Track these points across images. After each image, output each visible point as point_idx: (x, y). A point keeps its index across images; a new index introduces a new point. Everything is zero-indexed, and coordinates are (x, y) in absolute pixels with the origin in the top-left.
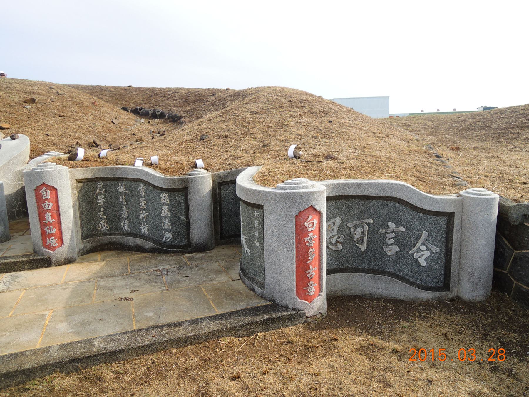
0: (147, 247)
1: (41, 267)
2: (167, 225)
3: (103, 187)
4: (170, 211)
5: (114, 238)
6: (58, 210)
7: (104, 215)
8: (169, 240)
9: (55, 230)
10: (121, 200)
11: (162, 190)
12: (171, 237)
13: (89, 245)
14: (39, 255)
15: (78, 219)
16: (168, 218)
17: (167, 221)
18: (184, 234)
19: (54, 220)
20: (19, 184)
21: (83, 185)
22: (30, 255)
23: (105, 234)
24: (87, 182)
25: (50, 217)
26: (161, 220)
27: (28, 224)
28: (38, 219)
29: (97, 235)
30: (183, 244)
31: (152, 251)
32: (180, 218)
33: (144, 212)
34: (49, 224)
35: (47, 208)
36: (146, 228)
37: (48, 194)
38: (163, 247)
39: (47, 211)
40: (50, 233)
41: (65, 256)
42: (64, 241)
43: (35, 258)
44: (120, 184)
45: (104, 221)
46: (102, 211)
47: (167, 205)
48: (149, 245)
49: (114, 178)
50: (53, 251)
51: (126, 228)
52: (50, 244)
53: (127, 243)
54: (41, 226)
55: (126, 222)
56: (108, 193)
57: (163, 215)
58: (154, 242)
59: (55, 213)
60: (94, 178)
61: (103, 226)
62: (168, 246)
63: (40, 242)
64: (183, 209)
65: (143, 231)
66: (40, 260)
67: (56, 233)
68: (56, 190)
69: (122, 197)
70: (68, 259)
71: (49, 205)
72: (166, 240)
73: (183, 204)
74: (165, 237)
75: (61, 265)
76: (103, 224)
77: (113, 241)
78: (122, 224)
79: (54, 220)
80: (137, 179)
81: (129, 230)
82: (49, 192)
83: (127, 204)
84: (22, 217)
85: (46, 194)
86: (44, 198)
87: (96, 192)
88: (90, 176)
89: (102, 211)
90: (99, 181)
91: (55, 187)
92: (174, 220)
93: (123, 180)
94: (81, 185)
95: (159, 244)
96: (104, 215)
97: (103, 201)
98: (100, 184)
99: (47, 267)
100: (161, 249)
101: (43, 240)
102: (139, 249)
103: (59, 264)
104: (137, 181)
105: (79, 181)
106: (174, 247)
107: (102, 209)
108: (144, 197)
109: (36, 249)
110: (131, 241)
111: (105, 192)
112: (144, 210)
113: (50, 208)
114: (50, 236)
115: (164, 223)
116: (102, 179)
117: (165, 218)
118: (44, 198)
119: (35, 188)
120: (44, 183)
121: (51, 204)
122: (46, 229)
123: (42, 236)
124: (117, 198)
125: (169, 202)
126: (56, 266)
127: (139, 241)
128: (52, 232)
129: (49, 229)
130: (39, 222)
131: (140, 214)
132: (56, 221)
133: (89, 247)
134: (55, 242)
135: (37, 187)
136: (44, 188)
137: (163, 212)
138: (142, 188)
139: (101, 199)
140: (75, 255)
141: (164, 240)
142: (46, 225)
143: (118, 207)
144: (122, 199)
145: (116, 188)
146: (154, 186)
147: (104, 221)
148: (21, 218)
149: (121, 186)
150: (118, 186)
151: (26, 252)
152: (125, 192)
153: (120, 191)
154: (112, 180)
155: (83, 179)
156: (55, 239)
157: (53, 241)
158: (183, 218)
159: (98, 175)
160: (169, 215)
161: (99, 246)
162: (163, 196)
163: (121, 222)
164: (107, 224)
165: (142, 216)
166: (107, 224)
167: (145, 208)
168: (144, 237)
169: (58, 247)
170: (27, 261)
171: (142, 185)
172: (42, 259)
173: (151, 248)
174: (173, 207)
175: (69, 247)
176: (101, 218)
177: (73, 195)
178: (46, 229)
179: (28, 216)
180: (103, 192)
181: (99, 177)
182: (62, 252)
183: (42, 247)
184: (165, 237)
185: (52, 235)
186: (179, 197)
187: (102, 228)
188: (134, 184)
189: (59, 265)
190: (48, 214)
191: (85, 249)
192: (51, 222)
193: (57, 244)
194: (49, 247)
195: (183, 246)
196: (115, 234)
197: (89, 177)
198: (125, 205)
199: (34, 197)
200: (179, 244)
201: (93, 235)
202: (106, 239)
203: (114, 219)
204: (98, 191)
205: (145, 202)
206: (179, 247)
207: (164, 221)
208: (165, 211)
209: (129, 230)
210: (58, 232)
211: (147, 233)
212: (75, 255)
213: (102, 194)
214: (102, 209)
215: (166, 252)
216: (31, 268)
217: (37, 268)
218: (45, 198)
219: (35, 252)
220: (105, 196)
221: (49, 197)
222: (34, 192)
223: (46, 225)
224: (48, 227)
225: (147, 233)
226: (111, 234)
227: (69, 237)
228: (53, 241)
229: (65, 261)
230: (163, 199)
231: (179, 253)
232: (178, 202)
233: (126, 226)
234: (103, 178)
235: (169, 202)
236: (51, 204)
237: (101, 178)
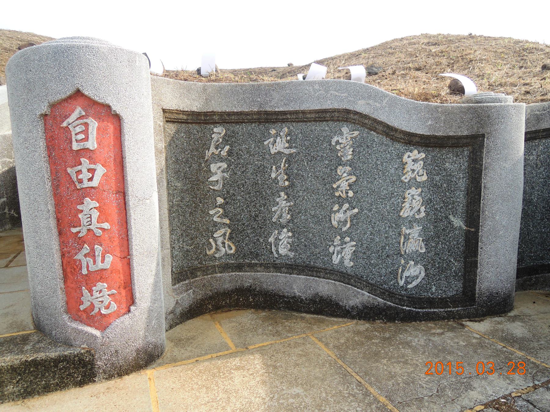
0: (352, 303)
1: (61, 386)
2: (414, 242)
3: (226, 140)
4: (427, 202)
5: (247, 278)
6: (122, 193)
7: (225, 215)
8: (414, 283)
9: (109, 258)
10: (273, 175)
11: (412, 140)
12: (423, 274)
13: (187, 298)
14: (55, 342)
15: (166, 224)
16: (418, 221)
17: (415, 232)
18: (457, 265)
19: (106, 226)
20: (4, 163)
21: (177, 132)
22: (25, 339)
23: (225, 268)
24: (186, 122)
25: (95, 214)
26: (398, 226)
27: (21, 241)
28: (52, 223)
29: (205, 270)
30: (450, 294)
31: (366, 313)
32: (450, 222)
33: (346, 206)
34: (93, 239)
35: (86, 184)
36: (349, 249)
37: (90, 135)
38: (401, 301)
39: (88, 192)
40: (92, 268)
41: (139, 343)
42: (137, 295)
43: (41, 356)
44: (273, 132)
45: (222, 231)
46: (220, 206)
47: (418, 185)
48: (359, 297)
49: (259, 113)
50: (103, 328)
51: (283, 251)
52: (92, 306)
53: (287, 291)
54: (63, 244)
55: (285, 235)
56: (239, 157)
57: (404, 214)
58: (373, 288)
59: (112, 199)
60: (206, 114)
61: (221, 245)
62: (415, 300)
63: (59, 300)
64: (461, 197)
65: (336, 260)
66: (57, 361)
67: (113, 270)
68: (117, 118)
69: (278, 168)
70: (146, 352)
71: (92, 171)
72: (407, 283)
73: (462, 184)
74: (406, 274)
75: (127, 372)
76: (220, 240)
77: (247, 285)
78: (271, 240)
79: (106, 226)
80: (334, 111)
81: (292, 254)
82: (94, 125)
83: (292, 186)
84: (8, 226)
85: (86, 132)
86: (75, 146)
87: (208, 154)
88: (196, 106)
89: (220, 206)
90: (215, 123)
91: (117, 108)
92: (435, 228)
93: (283, 121)
94: (172, 128)
95: (389, 294)
96: (225, 215)
97: (224, 179)
98: (219, 132)
99: (81, 384)
100: (395, 310)
101: (67, 293)
102: (325, 308)
103: (121, 371)
104: (324, 120)
105: (171, 117)
106: (431, 302)
107: (220, 200)
108: (351, 163)
109: (46, 321)
110: (299, 285)
111: (230, 153)
112: (347, 200)
113: (95, 183)
114: (91, 279)
115: (407, 237)
116: (225, 119)
117: (411, 222)
118: (75, 146)
119: (44, 108)
120: (78, 93)
121: (100, 171)
122: (80, 256)
123: (65, 278)
124: (262, 170)
125: (425, 178)
126: (110, 377)
127: (325, 287)
128: (100, 265)
129: (92, 254)
130: (55, 231)
131: (331, 212)
132: (115, 229)
133: (186, 304)
134: (107, 300)
135: (53, 106)
136: (78, 111)
137: (407, 205)
138: (345, 137)
139: (218, 173)
140: (162, 337)
141: (402, 283)
142: (81, 241)
143: (263, 193)
144: (278, 175)
145: (261, 141)
146: (390, 132)
147: (222, 231)
148: (5, 230)
149: (277, 135)
150: (266, 135)
151: (11, 326)
152: (287, 151)
153: (273, 151)
154: (251, 122)
155: (179, 112)
156: (109, 288)
157: (102, 298)
158: (458, 222)
159: (219, 106)
160: (423, 214)
161: (211, 298)
162: (409, 161)
163: (269, 234)
164: (230, 239)
165: (338, 217)
166: (230, 239)
167: (351, 194)
168: (343, 276)
169: (117, 314)
170: (13, 369)
171: (345, 130)
172: (65, 359)
173: (365, 307)
174: (436, 191)
175: (150, 311)
176: (215, 224)
177: (158, 152)
178: (80, 256)
179: (21, 226)
180: (224, 153)
181: (218, 109)
182: (133, 328)
183: (66, 317)
184: (406, 274)
185: (101, 275)
186: (455, 164)
187: (217, 249)
188: (318, 128)
189: (120, 375)
190: (90, 204)
191: (179, 310)
192: (99, 232)
193: (114, 307)
194: (90, 317)
195: (454, 301)
196: (252, 267)
197: (195, 109)
198: (284, 189)
199: (42, 144)
200: (440, 294)
201: (196, 269)
202: (227, 280)
203: (250, 228)
204: (212, 149)
205: (354, 178)
206: (443, 302)
207: (405, 230)
208: (413, 204)
209: (292, 254)
210: (119, 265)
211: (348, 264)
212: (162, 337)
213: (221, 160)
214: (220, 200)
215: (409, 318)
216: (27, 393)
217: (47, 389)
218: (81, 146)
219: (39, 327)
220: (229, 166)
221: (92, 144)
222: (41, 123)
223: (81, 241)
224: (86, 248)
225: (348, 264)
226: (239, 267)
227: (151, 280)
228: (102, 298)
229: (136, 359)
230: (408, 168)
231: (443, 318)
232: (449, 178)
233: (283, 244)
234: (229, 114)
235: (425, 178)
236: (100, 171)
237: (221, 114)
